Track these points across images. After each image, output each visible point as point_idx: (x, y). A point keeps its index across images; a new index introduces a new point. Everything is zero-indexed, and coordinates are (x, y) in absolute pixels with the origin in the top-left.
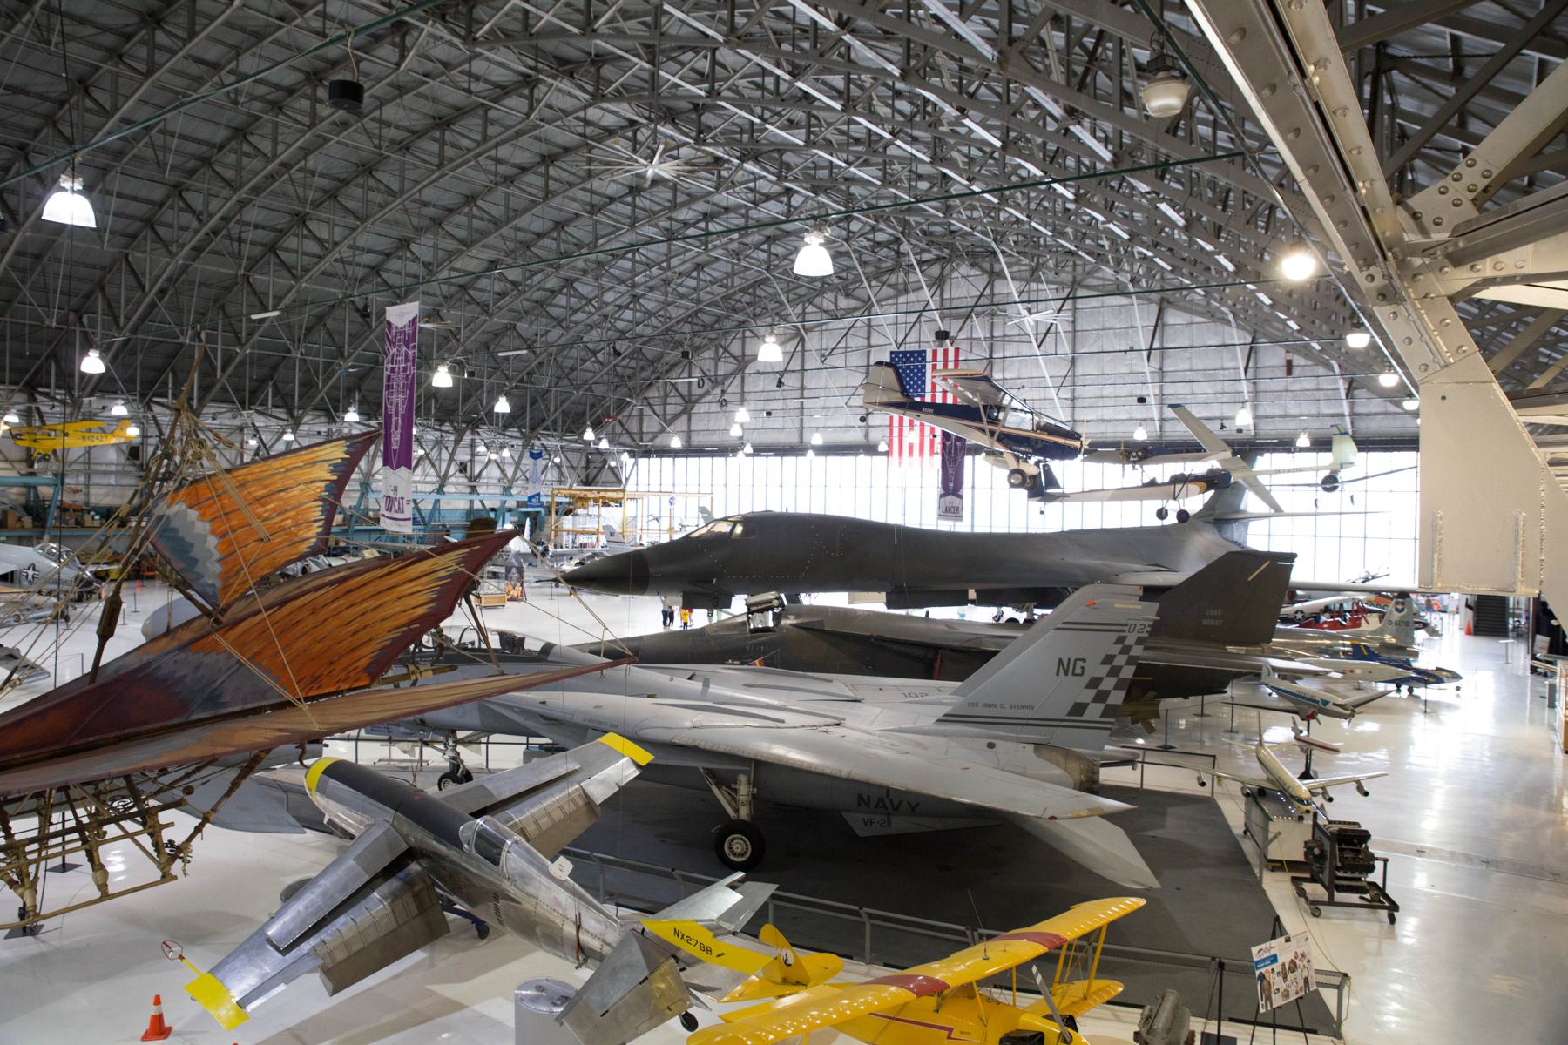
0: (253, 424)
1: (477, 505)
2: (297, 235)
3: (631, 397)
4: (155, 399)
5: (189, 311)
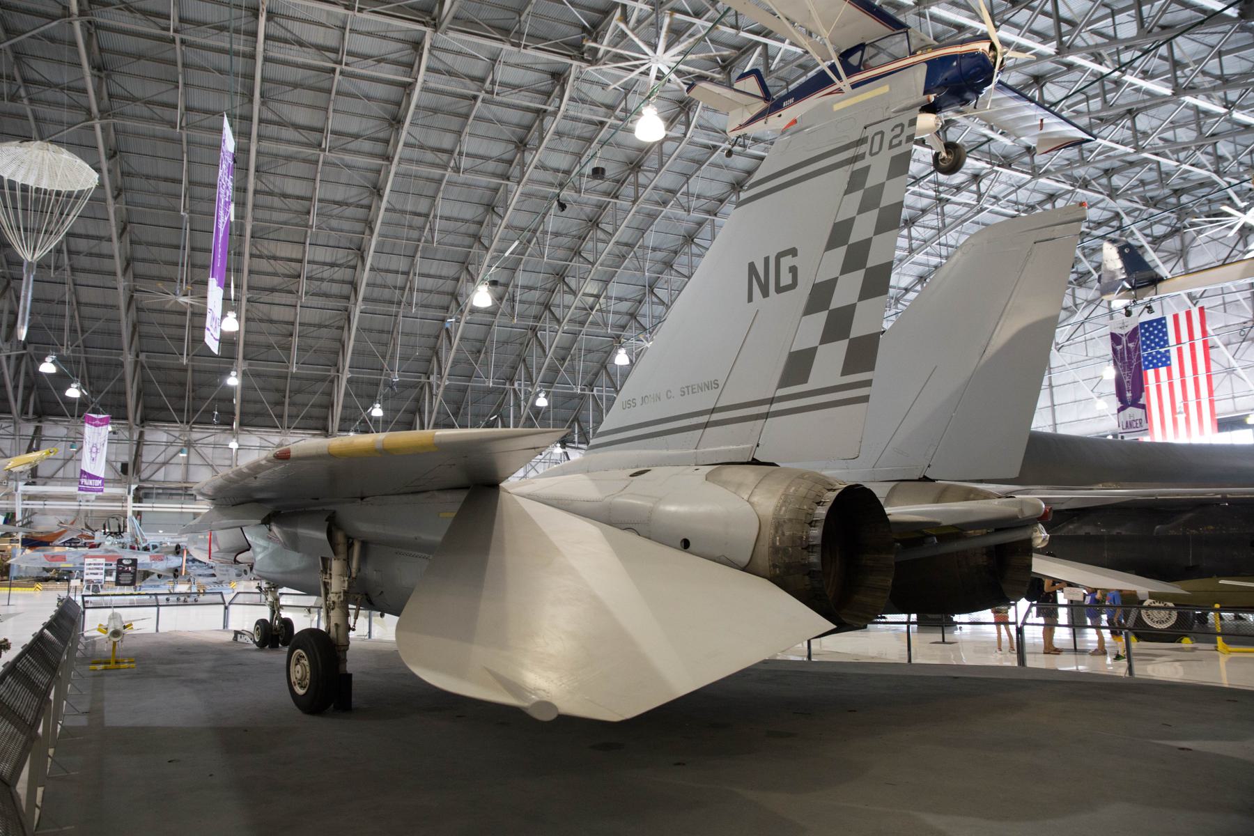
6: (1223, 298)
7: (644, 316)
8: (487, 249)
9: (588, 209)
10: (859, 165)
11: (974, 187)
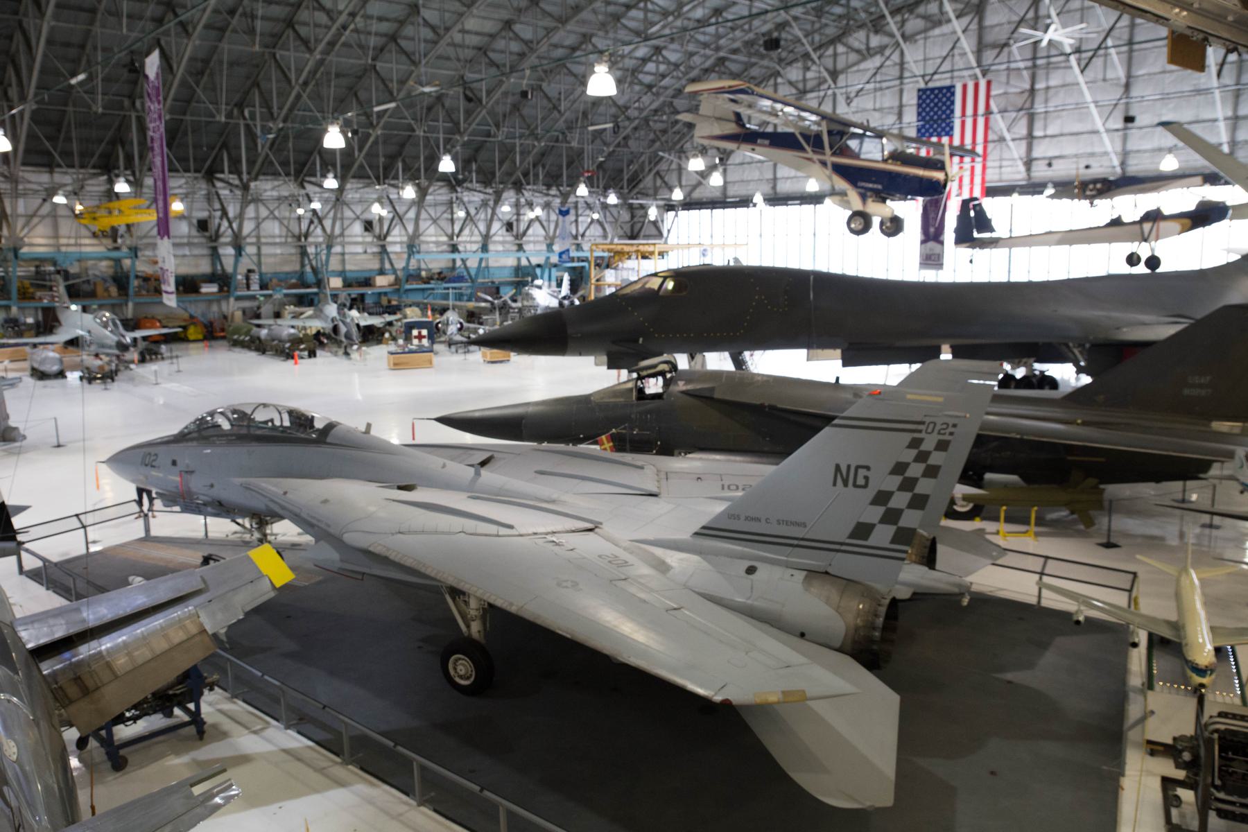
0: (388, 197)
1: (524, 262)
2: (504, 38)
3: (664, 151)
4: (307, 179)
10: (916, 435)
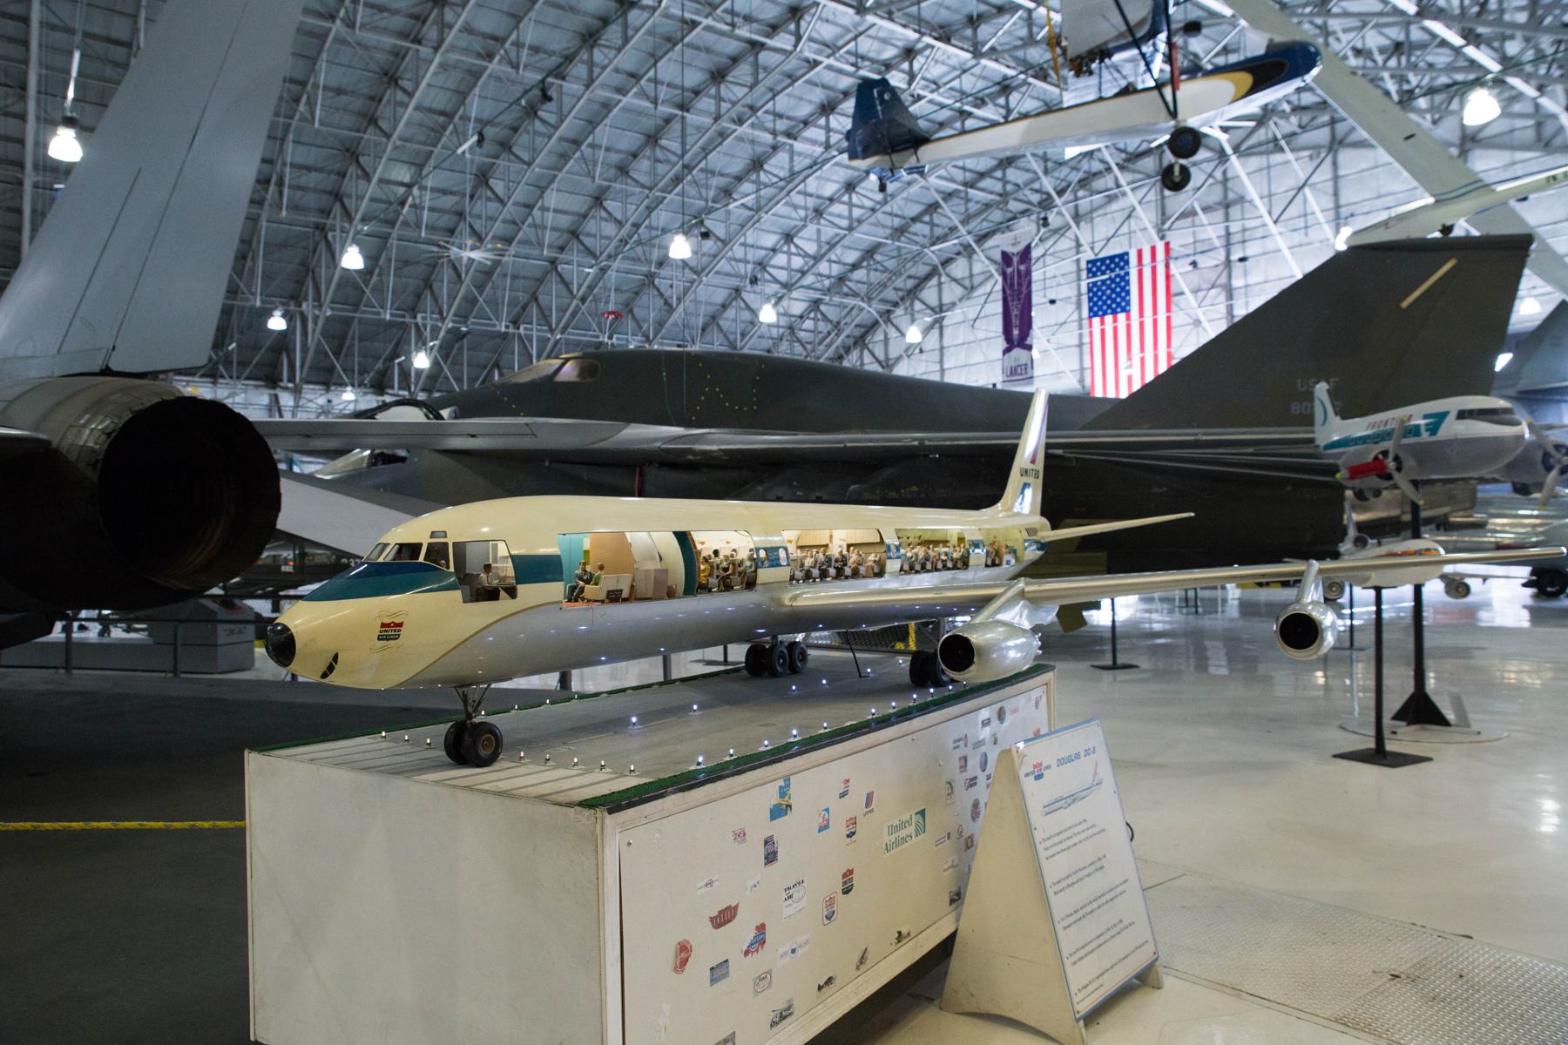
5: (503, 302)
6: (1194, 233)
7: (589, 235)
8: (388, 136)
9: (381, 57)
11: (905, 66)
